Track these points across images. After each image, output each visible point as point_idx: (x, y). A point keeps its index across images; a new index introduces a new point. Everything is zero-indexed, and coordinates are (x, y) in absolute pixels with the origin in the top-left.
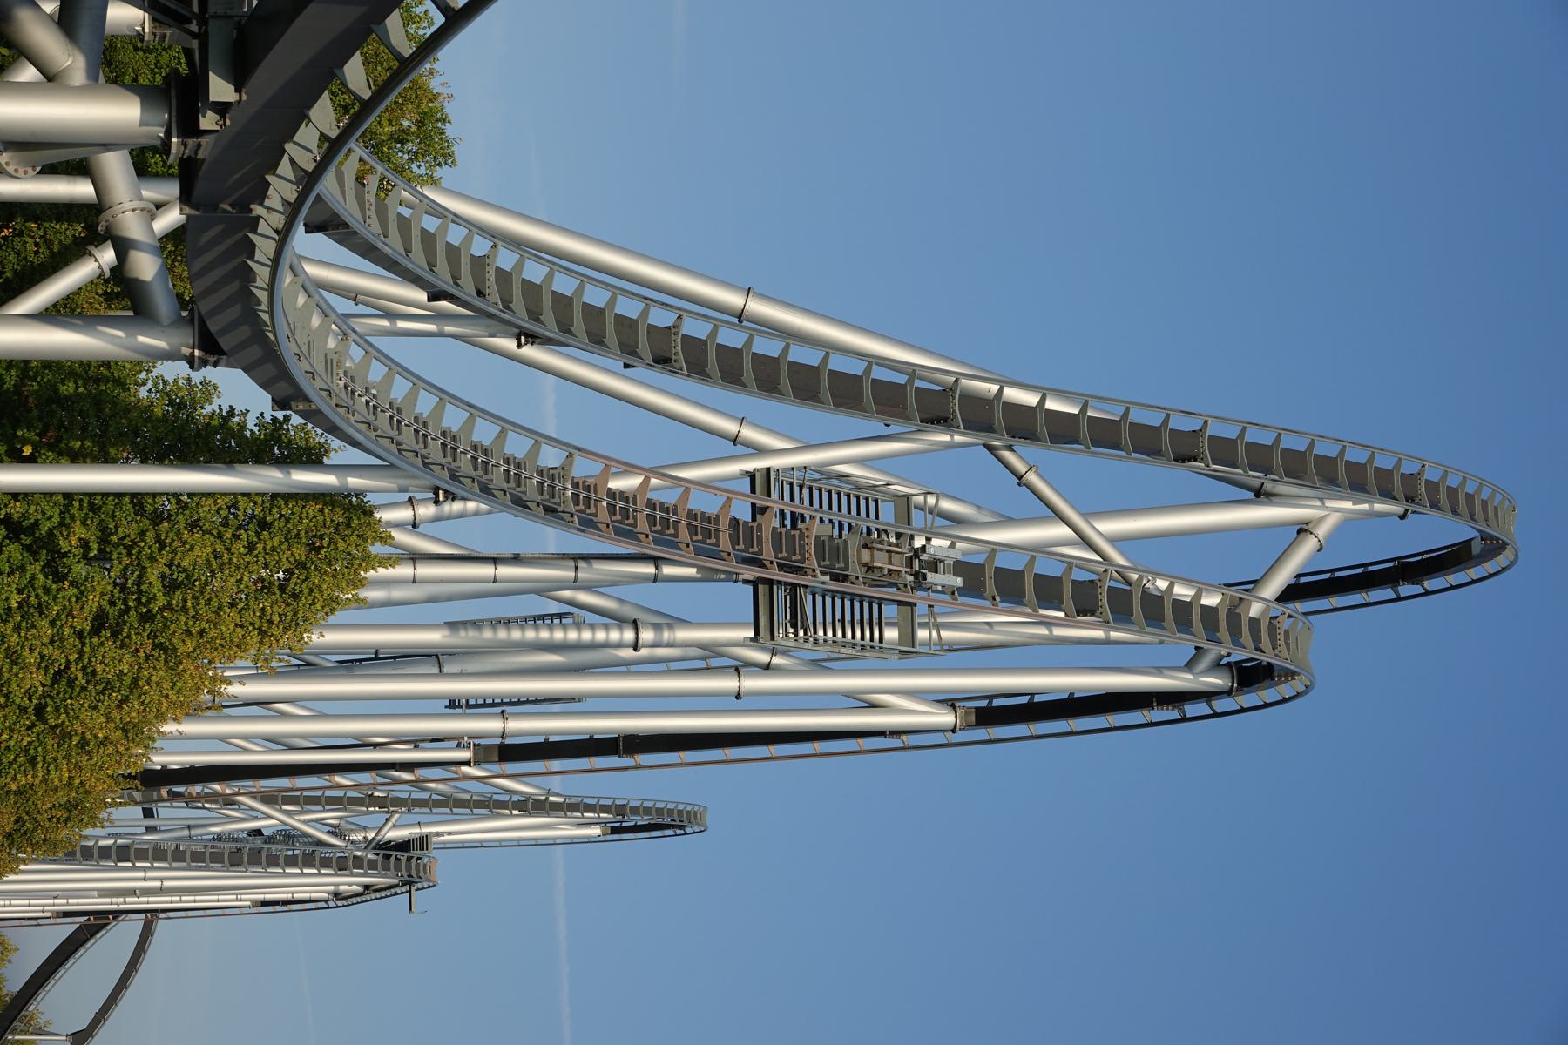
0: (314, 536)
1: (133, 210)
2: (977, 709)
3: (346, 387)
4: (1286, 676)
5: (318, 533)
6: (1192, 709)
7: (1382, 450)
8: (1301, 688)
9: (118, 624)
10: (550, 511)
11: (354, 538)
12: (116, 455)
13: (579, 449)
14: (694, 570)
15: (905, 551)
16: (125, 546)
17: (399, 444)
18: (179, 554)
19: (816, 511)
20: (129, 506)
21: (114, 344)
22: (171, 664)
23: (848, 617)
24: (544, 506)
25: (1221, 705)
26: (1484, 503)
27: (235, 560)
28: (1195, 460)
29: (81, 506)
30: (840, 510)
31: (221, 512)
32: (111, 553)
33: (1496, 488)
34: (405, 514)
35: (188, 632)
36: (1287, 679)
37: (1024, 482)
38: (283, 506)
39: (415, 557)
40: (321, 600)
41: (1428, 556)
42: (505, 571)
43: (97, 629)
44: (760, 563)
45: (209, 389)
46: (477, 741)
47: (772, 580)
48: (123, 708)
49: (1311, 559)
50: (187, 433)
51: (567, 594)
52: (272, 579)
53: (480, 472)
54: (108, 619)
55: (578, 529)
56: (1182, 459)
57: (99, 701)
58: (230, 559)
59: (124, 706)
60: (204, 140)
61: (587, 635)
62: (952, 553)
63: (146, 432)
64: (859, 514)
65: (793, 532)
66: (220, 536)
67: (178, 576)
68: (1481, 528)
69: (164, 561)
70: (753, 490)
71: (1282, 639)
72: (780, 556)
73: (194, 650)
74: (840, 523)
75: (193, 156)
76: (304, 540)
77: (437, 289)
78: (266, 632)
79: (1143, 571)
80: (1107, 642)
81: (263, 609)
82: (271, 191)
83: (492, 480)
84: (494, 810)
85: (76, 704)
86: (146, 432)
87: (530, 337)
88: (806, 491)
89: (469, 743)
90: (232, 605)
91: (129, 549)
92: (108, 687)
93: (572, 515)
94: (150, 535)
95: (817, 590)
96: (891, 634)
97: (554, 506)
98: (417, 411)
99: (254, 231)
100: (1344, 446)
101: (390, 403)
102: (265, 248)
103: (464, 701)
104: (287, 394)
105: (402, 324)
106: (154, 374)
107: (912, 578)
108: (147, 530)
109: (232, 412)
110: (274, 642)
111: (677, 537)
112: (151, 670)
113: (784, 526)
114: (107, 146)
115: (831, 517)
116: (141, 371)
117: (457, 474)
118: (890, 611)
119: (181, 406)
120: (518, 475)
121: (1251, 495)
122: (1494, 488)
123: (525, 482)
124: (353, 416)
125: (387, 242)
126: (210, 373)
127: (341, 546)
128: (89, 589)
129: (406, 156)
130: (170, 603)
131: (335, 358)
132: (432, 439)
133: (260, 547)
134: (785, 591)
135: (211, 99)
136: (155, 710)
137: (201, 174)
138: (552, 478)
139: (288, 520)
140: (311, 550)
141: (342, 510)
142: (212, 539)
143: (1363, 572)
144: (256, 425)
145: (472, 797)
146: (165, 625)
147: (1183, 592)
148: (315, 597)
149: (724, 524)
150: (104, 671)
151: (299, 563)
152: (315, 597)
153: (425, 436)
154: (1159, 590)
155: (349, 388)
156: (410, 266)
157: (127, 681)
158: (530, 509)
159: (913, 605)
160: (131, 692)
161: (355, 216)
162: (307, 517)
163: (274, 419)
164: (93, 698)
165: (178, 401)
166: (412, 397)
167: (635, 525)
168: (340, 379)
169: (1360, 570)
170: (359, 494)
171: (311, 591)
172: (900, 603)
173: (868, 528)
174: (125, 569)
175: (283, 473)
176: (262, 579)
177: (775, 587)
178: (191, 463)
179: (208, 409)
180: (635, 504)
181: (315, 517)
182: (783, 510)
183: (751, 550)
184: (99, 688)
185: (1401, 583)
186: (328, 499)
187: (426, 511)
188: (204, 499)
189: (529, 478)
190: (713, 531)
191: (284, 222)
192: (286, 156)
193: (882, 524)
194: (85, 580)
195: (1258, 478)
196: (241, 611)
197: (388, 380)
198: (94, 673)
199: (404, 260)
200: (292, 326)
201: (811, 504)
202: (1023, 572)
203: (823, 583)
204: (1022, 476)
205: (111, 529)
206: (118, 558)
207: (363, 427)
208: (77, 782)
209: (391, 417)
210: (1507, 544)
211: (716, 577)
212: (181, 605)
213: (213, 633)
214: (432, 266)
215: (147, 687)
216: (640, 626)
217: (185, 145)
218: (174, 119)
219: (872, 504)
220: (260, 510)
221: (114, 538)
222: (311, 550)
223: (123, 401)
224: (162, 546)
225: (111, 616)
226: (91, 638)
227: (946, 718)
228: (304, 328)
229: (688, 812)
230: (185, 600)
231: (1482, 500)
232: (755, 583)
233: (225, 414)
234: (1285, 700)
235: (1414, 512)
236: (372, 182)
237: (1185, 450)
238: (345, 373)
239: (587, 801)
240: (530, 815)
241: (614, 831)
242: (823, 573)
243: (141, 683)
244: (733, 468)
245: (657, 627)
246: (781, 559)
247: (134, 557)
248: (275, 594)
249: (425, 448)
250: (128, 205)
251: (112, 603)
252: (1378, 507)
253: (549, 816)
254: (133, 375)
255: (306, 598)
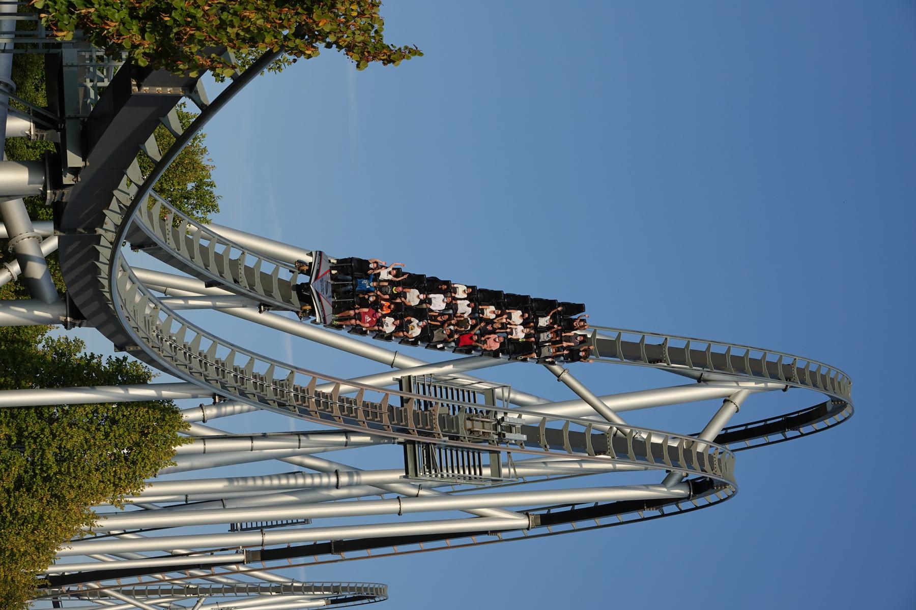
0: (144, 427)
1: (28, 238)
2: (541, 515)
3: (157, 336)
4: (721, 486)
5: (146, 425)
6: (667, 509)
7: (770, 351)
8: (730, 493)
9: (30, 484)
10: (281, 405)
11: (167, 427)
12: (25, 384)
13: (297, 368)
14: (369, 438)
15: (492, 421)
16: (32, 437)
17: (190, 369)
18: (64, 441)
19: (438, 399)
20: (34, 415)
21: (20, 317)
22: (62, 506)
23: (461, 464)
24: (278, 402)
25: (684, 506)
26: (832, 380)
27: (97, 443)
28: (661, 362)
29: (6, 415)
30: (453, 398)
31: (88, 415)
32: (24, 442)
33: (839, 371)
34: (198, 414)
35: (71, 487)
36: (721, 488)
37: (561, 379)
38: (125, 410)
39: (204, 439)
40: (149, 464)
41: (802, 413)
42: (257, 444)
43: (18, 487)
44: (406, 431)
45: (79, 344)
46: (248, 549)
47: (414, 441)
48: (35, 533)
49: (732, 418)
50: (67, 370)
51: (297, 459)
52: (120, 453)
53: (239, 384)
54: (24, 481)
55: (299, 415)
56: (653, 361)
57: (21, 529)
58: (95, 443)
59: (36, 532)
60: (66, 191)
61: (309, 481)
62: (519, 421)
63: (43, 370)
64: (464, 400)
65: (425, 413)
66: (88, 430)
67: (65, 454)
68: (831, 394)
69: (56, 445)
70: (401, 389)
71: (717, 464)
72: (418, 426)
73: (76, 497)
74: (453, 406)
75: (60, 200)
76: (138, 430)
77: (210, 280)
78: (118, 485)
79: (632, 427)
80: (615, 470)
81: (115, 471)
82: (107, 219)
83: (246, 388)
84: (261, 593)
85: (7, 532)
86: (43, 370)
87: (264, 306)
88: (432, 389)
89: (243, 551)
90: (97, 470)
91: (35, 439)
92: (25, 521)
93: (295, 408)
94: (47, 431)
95: (441, 446)
96: (487, 472)
97: (284, 402)
98: (200, 349)
99: (98, 244)
100: (748, 350)
101: (184, 345)
102: (105, 254)
103: (239, 524)
104: (123, 341)
105: (191, 302)
106: (46, 336)
107: (497, 437)
108: (45, 428)
109: (92, 357)
110: (123, 490)
111: (357, 418)
112: (50, 510)
113: (420, 409)
114: (10, 197)
115: (448, 403)
116: (38, 335)
117: (226, 385)
118: (485, 458)
119: (62, 355)
120: (262, 385)
121: (695, 381)
122: (837, 371)
123: (266, 389)
124: (163, 353)
125: (180, 253)
126: (78, 333)
127: (160, 432)
128: (12, 464)
129: (190, 207)
130: (60, 470)
131: (150, 319)
132: (210, 365)
133: (112, 435)
134: (423, 447)
135: (69, 166)
136: (53, 533)
137: (65, 211)
138: (282, 386)
139: (128, 419)
140: (142, 435)
141: (159, 411)
142: (84, 431)
143: (764, 425)
144: (107, 363)
145: (247, 586)
146: (58, 483)
147: (656, 440)
148: (145, 463)
149: (385, 409)
150: (23, 511)
151: (136, 444)
152: (145, 463)
153: (206, 364)
154: (643, 438)
155: (159, 337)
156: (194, 267)
157: (37, 517)
158: (269, 404)
159: (498, 452)
160: (39, 523)
161: (160, 238)
162: (139, 416)
163: (118, 359)
164: (17, 528)
165: (60, 351)
166: (197, 341)
167: (332, 412)
168: (154, 331)
169: (762, 424)
170: (169, 401)
171: (143, 459)
172: (491, 452)
173: (470, 408)
174: (34, 450)
175: (124, 391)
176: (114, 454)
177: (416, 445)
178: (70, 386)
179: (79, 355)
180: (331, 399)
181: (144, 415)
182: (419, 400)
183: (401, 424)
184: (20, 522)
185: (787, 430)
186: (151, 405)
187: (211, 412)
188: (78, 408)
189: (268, 386)
190: (378, 414)
191: (114, 237)
192: (114, 198)
193: (478, 405)
194: (10, 459)
195: (698, 370)
196: (102, 473)
197: (182, 332)
198: (17, 513)
199: (189, 263)
200: (124, 301)
201: (436, 396)
202: (562, 430)
203: (445, 441)
204: (560, 376)
205: (24, 428)
206: (29, 445)
207: (169, 359)
208: (9, 578)
209: (185, 353)
210: (847, 404)
211: (382, 441)
212: (66, 471)
213: (86, 486)
214: (206, 266)
215: (48, 520)
216: (339, 474)
217: (55, 194)
218: (48, 180)
219: (472, 395)
220: (111, 413)
221: (26, 434)
222: (142, 435)
223: (29, 353)
224: (54, 436)
225: (26, 480)
226: (14, 493)
227: (523, 522)
228: (131, 302)
229: (376, 589)
230: (69, 468)
231: (831, 378)
232: (405, 444)
233: (88, 358)
234: (721, 501)
235: (791, 387)
236: (169, 219)
237: (654, 356)
238: (157, 328)
239: (316, 585)
240: (282, 595)
241: (333, 602)
242: (444, 436)
243: (45, 518)
244: (389, 379)
245: (350, 474)
246: (419, 428)
247: (38, 444)
248: (122, 462)
249: (206, 370)
250: (25, 235)
251: (26, 472)
252: (770, 385)
253: (293, 594)
254: (33, 337)
255: (140, 463)
